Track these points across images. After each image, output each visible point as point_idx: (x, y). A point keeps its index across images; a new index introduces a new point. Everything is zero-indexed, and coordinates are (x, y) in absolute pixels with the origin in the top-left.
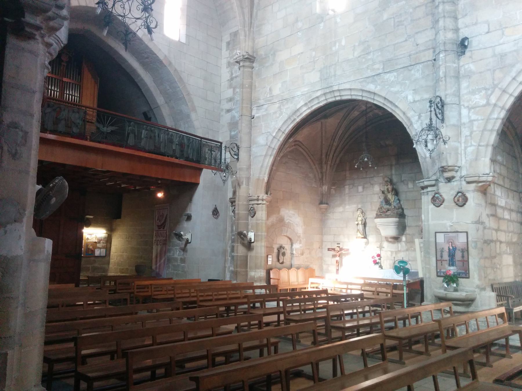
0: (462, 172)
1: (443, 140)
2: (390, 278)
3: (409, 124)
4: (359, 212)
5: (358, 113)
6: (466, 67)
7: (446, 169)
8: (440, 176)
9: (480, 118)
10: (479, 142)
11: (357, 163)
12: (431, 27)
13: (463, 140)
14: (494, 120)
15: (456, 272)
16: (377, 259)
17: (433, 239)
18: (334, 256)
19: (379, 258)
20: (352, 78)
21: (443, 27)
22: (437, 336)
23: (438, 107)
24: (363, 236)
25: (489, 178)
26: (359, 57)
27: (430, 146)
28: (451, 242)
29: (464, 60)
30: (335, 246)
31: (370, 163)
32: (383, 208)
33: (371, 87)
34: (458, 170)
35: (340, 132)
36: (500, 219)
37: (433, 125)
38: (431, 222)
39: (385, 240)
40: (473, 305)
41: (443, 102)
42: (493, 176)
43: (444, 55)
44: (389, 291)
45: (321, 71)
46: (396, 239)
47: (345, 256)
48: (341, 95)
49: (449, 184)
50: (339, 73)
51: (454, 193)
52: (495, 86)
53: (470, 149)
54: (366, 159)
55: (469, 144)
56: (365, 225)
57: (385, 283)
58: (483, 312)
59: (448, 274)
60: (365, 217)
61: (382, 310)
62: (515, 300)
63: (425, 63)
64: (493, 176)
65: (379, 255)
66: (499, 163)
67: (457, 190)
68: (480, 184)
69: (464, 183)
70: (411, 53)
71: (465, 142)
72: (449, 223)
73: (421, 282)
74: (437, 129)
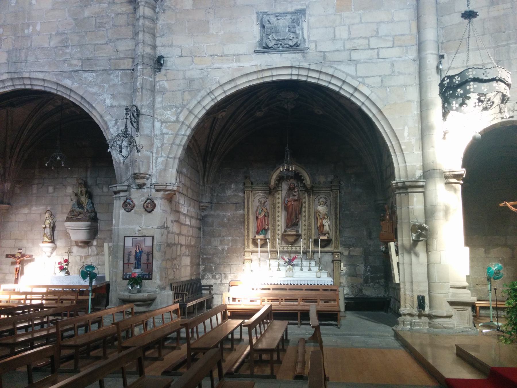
0: (152, 180)
1: (137, 148)
2: (77, 285)
3: (105, 128)
4: (47, 215)
5: (53, 108)
6: (161, 83)
7: (138, 176)
8: (132, 182)
9: (170, 133)
10: (169, 154)
11: (48, 161)
12: (132, 37)
13: (155, 151)
14: (182, 136)
15: (140, 274)
16: (64, 264)
17: (121, 243)
18: (13, 263)
19: (66, 263)
20: (46, 68)
21: (142, 41)
22: (116, 339)
23: (133, 116)
24: (50, 241)
25: (174, 187)
26: (56, 48)
27: (124, 152)
28: (138, 246)
29: (159, 76)
30: (16, 252)
31: (63, 163)
32: (74, 211)
33: (67, 82)
34: (149, 178)
35: (30, 125)
36: (182, 224)
37: (128, 133)
38: (121, 227)
39: (75, 245)
40: (153, 305)
41: (138, 112)
42: (178, 186)
43: (142, 67)
44: (74, 298)
45: (8, 52)
46: (87, 243)
47: (27, 263)
48: (32, 84)
49: (140, 190)
50: (30, 59)
51: (144, 199)
52: (184, 106)
53: (160, 160)
54: (58, 158)
55: (160, 155)
56: (53, 228)
57: (71, 289)
58: (160, 310)
59: (133, 276)
60: (54, 220)
61: (62, 318)
62: (190, 296)
63: (124, 71)
64: (178, 186)
65: (66, 261)
66: (185, 175)
67: (147, 196)
68: (167, 193)
69: (153, 190)
70: (111, 57)
71: (156, 153)
72: (137, 228)
73: (108, 285)
74: (132, 137)
